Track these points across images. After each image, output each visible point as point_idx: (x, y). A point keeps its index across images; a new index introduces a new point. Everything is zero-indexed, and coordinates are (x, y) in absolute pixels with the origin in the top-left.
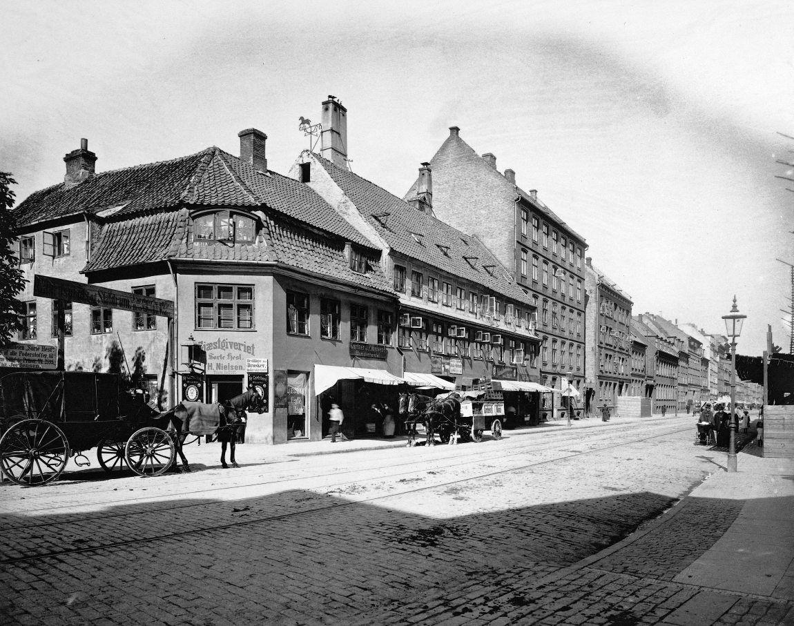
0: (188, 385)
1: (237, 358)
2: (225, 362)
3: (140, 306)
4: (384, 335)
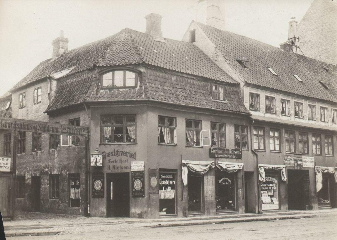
0: (136, 179)
1: (125, 162)
2: (118, 164)
3: (66, 131)
4: (165, 130)
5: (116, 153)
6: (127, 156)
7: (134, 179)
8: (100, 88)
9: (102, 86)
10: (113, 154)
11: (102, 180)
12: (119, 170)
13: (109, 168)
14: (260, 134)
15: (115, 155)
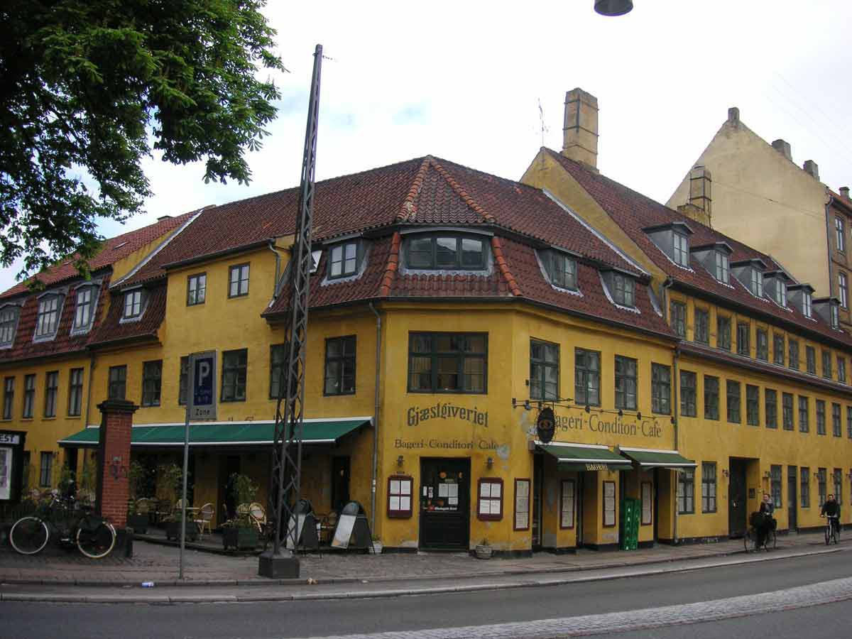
10: (436, 412)
14: (662, 380)
15: (440, 414)
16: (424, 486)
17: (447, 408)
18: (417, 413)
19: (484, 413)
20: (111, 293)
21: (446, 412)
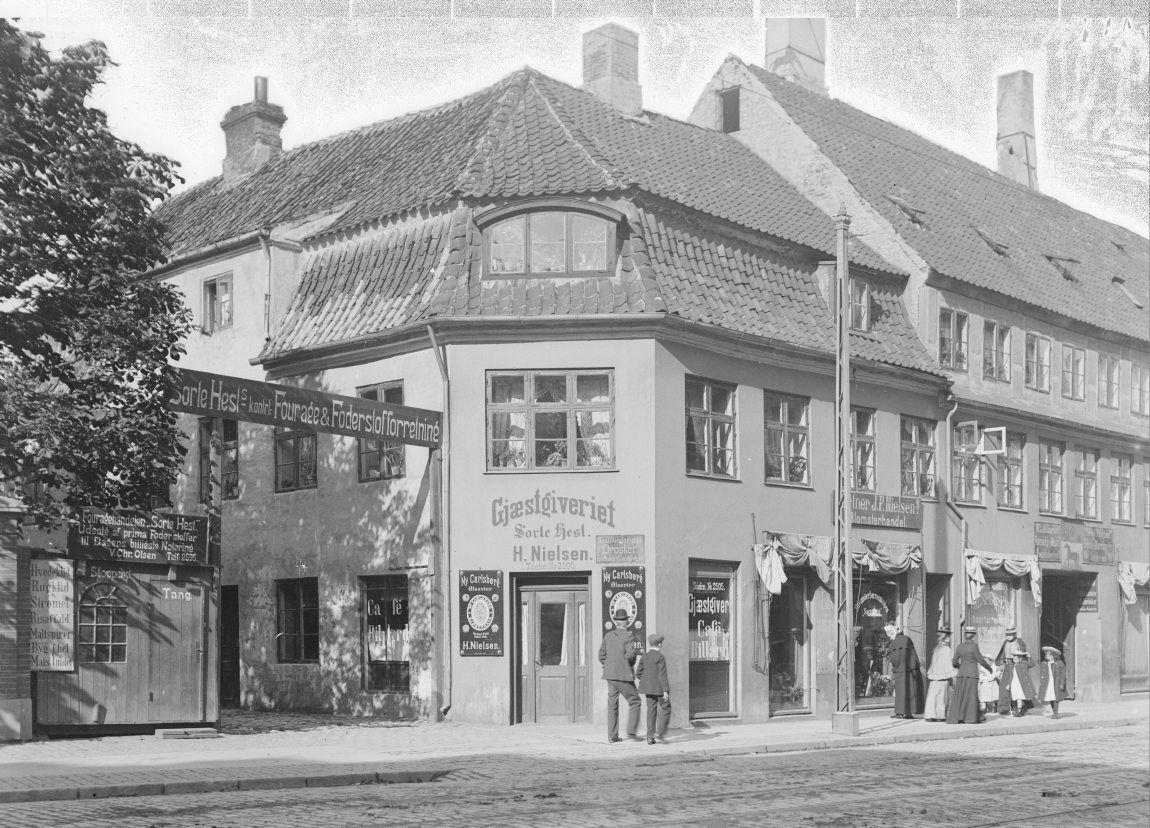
5: (543, 505)
6: (582, 514)
7: (608, 594)
8: (480, 277)
9: (487, 267)
10: (534, 507)
11: (495, 597)
12: (555, 561)
13: (518, 556)
16: (497, 633)
17: (551, 501)
18: (506, 507)
19: (606, 504)
20: (714, 410)
21: (549, 507)
